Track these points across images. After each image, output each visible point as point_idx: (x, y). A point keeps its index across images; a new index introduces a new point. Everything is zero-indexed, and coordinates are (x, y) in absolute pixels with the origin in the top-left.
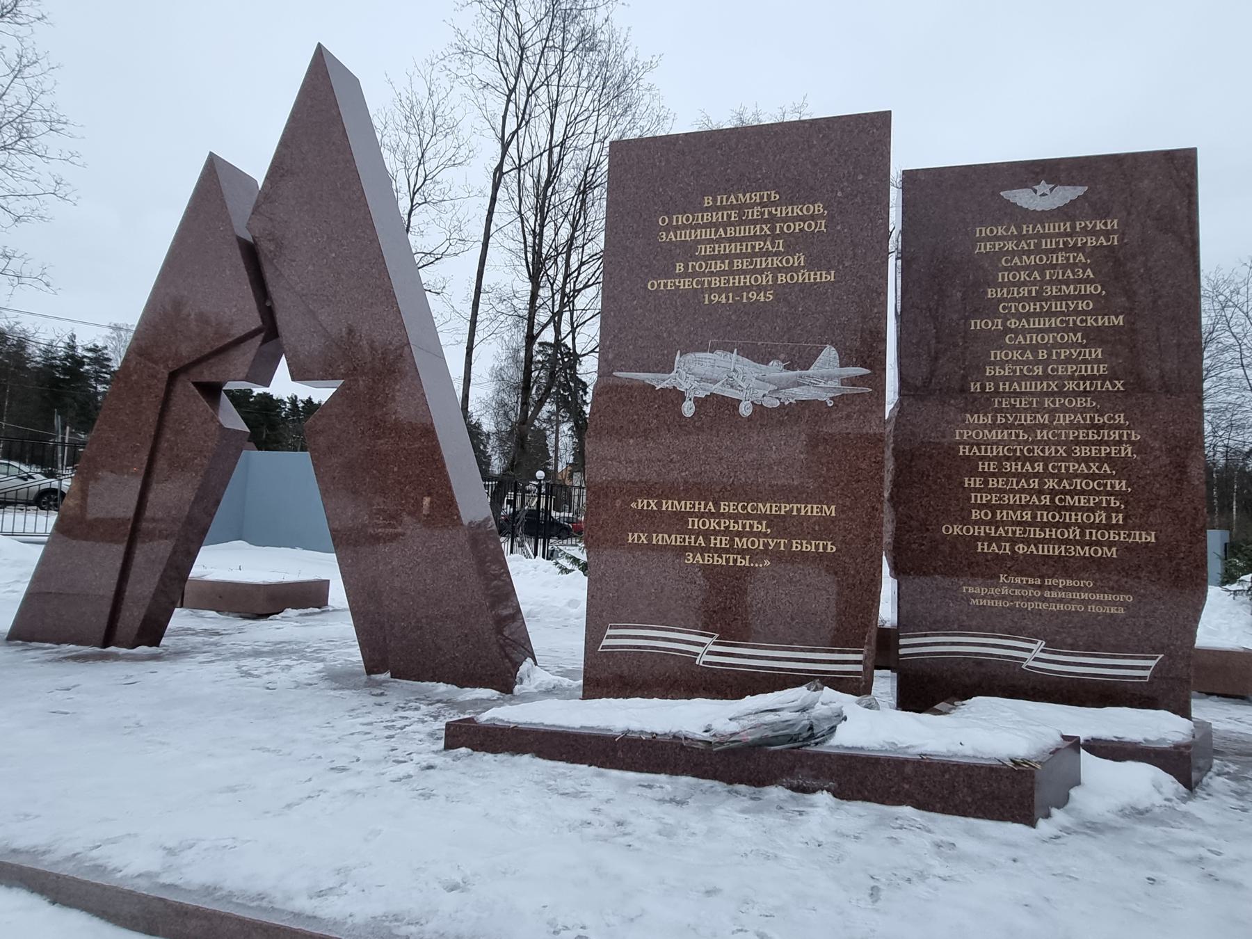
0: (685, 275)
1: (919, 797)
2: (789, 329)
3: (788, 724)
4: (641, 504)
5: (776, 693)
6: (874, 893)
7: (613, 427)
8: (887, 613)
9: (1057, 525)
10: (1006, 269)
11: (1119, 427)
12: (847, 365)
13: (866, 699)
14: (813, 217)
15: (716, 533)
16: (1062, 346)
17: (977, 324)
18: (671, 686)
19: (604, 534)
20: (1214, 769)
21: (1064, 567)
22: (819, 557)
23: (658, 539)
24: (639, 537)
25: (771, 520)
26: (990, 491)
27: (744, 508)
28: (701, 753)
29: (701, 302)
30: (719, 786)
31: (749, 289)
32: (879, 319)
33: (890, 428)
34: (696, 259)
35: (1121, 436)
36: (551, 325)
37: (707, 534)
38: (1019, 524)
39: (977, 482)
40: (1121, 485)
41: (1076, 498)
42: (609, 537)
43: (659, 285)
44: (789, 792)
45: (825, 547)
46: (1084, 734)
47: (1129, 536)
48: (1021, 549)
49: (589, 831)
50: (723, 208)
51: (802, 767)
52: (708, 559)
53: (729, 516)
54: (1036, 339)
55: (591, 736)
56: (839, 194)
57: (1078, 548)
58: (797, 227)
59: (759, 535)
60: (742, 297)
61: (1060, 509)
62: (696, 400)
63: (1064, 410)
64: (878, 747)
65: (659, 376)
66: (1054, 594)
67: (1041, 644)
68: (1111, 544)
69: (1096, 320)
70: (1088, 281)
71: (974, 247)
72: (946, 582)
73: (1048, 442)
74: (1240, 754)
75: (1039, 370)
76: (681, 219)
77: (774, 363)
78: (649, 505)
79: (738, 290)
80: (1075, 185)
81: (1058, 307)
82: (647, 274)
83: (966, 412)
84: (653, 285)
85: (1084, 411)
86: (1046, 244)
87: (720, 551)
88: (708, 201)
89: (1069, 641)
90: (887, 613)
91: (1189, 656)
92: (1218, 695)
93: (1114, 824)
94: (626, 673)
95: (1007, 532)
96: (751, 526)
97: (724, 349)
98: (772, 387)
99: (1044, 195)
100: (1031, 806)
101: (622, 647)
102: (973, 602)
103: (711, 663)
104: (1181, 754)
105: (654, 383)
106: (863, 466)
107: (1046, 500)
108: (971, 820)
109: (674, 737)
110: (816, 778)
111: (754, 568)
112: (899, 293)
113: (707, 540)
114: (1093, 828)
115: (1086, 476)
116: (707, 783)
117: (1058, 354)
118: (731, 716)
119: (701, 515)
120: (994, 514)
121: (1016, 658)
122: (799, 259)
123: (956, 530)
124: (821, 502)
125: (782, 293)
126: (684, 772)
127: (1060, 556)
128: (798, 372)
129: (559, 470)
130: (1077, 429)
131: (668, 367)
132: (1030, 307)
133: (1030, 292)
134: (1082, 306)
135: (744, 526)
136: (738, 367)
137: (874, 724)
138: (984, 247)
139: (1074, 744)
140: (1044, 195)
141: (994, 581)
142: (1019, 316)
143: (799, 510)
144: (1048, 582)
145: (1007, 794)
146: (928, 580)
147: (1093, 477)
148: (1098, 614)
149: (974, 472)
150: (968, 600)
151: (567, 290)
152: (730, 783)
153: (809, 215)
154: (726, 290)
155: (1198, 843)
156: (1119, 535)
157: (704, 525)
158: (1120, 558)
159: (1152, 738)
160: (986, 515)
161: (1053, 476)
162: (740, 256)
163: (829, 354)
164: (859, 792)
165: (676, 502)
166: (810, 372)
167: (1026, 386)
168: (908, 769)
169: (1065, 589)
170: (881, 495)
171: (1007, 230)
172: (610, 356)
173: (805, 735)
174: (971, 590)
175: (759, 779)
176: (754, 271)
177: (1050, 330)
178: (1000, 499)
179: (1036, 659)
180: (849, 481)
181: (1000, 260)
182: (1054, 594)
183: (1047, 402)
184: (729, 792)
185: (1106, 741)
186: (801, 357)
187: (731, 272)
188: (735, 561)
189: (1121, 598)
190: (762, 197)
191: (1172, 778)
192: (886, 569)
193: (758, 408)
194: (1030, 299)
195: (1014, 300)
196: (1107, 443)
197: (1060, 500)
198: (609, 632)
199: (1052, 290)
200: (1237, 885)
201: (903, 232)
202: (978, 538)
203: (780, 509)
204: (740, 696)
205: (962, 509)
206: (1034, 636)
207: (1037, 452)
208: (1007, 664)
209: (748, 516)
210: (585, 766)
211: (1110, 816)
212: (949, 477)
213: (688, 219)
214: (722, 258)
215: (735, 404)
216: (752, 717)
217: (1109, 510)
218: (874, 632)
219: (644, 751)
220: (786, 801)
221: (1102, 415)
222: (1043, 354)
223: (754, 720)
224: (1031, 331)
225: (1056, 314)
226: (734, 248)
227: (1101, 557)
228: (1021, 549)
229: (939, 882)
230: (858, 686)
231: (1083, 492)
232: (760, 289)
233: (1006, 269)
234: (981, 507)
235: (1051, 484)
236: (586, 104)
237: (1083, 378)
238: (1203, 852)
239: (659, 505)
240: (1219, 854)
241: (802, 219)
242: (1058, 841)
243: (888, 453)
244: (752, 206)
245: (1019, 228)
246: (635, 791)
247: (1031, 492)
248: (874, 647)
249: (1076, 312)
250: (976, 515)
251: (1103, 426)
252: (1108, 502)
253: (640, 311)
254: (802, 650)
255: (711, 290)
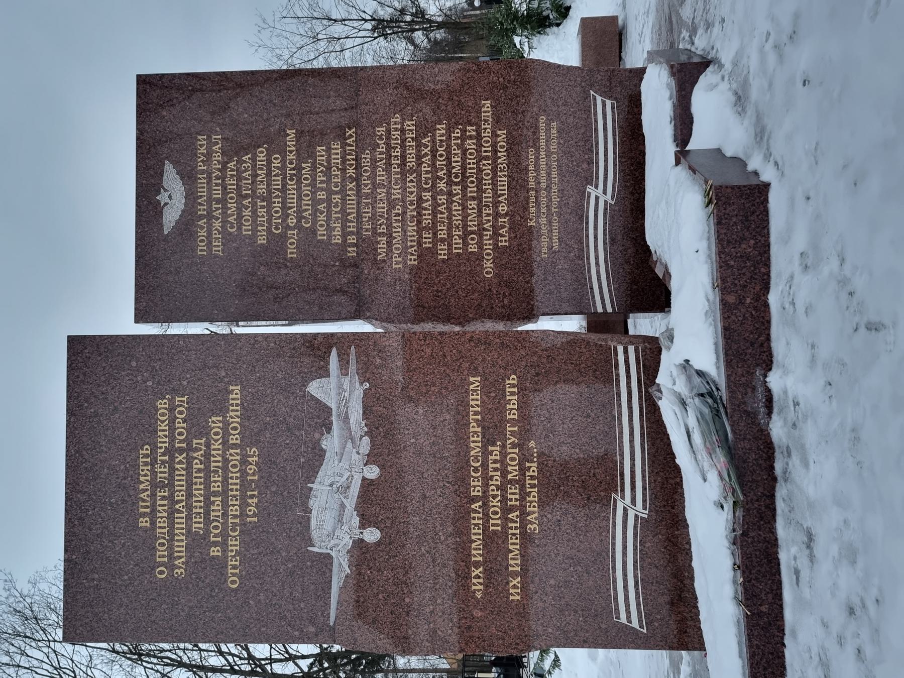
0: (224, 545)
1: (758, 288)
2: (289, 429)
3: (701, 418)
4: (477, 586)
5: (669, 431)
6: (873, 327)
7: (392, 623)
8: (573, 324)
9: (480, 180)
10: (239, 228)
11: (389, 132)
12: (328, 371)
13: (663, 342)
14: (172, 410)
15: (504, 500)
16: (314, 180)
17: (292, 251)
18: (675, 544)
19: (512, 629)
20: (689, 47)
21: (517, 171)
22: (522, 390)
23: (515, 564)
24: (514, 587)
25: (487, 442)
26: (450, 236)
27: (476, 470)
28: (747, 511)
29: (255, 526)
30: (781, 492)
31: (243, 473)
32: (765, 312)
33: (392, 327)
34: (207, 532)
35: (396, 130)
36: (297, 661)
37: (507, 510)
38: (480, 211)
39: (442, 249)
40: (441, 129)
41: (453, 164)
42: (515, 623)
43: (234, 575)
44: (775, 416)
45: (513, 386)
46: (671, 149)
47: (486, 121)
48: (503, 208)
49: (869, 651)
50: (153, 507)
51: (745, 403)
52: (533, 509)
53: (486, 485)
54: (306, 200)
55: (750, 646)
56: (150, 383)
57: (499, 161)
58: (180, 425)
59: (504, 454)
60: (252, 481)
61: (464, 177)
62: (363, 526)
63: (374, 175)
64: (712, 329)
65: (335, 569)
66: (543, 180)
67: (590, 189)
68: (494, 135)
69: (291, 152)
70: (254, 159)
71: (216, 256)
72: (538, 272)
73: (404, 189)
74: (671, 30)
75: (337, 198)
76: (161, 553)
77: (324, 444)
78: (478, 577)
79: (245, 485)
80: (163, 171)
81: (277, 183)
82: (221, 589)
83: (375, 259)
84: (233, 582)
85: (374, 161)
86: (218, 194)
87: (524, 495)
88: (144, 522)
89: (585, 166)
90: (573, 324)
91: (590, 70)
92: (620, 52)
93: (754, 118)
94: (667, 598)
95: (489, 221)
96: (495, 462)
97: (308, 497)
98: (349, 445)
99: (170, 197)
100: (751, 188)
101: (638, 604)
102: (556, 247)
103: (644, 501)
104: (679, 71)
105: (343, 575)
106: (428, 351)
107: (457, 189)
108: (773, 239)
109: (734, 544)
110: (754, 389)
111: (539, 457)
112: (264, 323)
113: (512, 509)
114: (761, 134)
115: (434, 157)
116: (780, 505)
117: (322, 182)
118: (702, 481)
119: (486, 517)
120: (472, 232)
121: (605, 209)
122: (215, 423)
123: (488, 265)
124: (467, 392)
125: (249, 438)
126: (773, 531)
127: (508, 176)
128: (334, 418)
129: (447, 666)
130: (391, 165)
131: (327, 560)
132: (277, 206)
133: (262, 207)
134: (277, 163)
135: (496, 470)
136: (328, 482)
137: (690, 333)
138: (217, 246)
139: (682, 155)
140: (170, 197)
141: (535, 230)
142: (286, 216)
143: (476, 413)
144: (532, 184)
145: (740, 212)
146: (537, 291)
147: (434, 152)
148: (559, 143)
149: (433, 251)
150: (555, 252)
151: (248, 668)
152: (775, 479)
153: (169, 414)
154: (244, 499)
155: (761, 50)
156: (485, 129)
157: (496, 513)
158: (507, 127)
159: (668, 94)
160: (473, 239)
161: (434, 186)
162: (207, 484)
163: (315, 388)
164: (762, 345)
165: (473, 545)
166: (333, 405)
167: (352, 208)
168: (731, 299)
169: (537, 170)
170: (458, 334)
171: (202, 228)
172: (312, 629)
173: (710, 401)
174: (544, 250)
175: (767, 449)
176: (225, 469)
177: (299, 189)
178: (457, 227)
179: (605, 192)
180: (445, 365)
181: (231, 233)
182: (543, 180)
183: (366, 190)
184: (786, 481)
185: (675, 130)
186: (318, 417)
187: (225, 493)
188: (532, 477)
189: (542, 126)
190: (146, 464)
191: (702, 77)
192: (519, 329)
193: (371, 458)
194: (269, 207)
195: (269, 221)
196: (404, 141)
197: (456, 177)
198: (623, 619)
199: (262, 189)
200: (797, 16)
201: (211, 321)
202: (496, 247)
203: (476, 432)
204: (677, 470)
205: (468, 260)
206: (583, 195)
207: (413, 198)
208: (612, 217)
209: (485, 465)
210: (787, 653)
211: (746, 122)
212: (439, 273)
213: (163, 545)
214: (208, 503)
215: (367, 484)
216: (699, 457)
217: (463, 138)
218: (594, 337)
219: (757, 579)
220: (785, 420)
221: (378, 145)
222: (322, 195)
223: (703, 455)
224: (299, 206)
225: (284, 185)
226: (199, 492)
227: (507, 143)
228: (503, 208)
229: (847, 266)
230: (651, 352)
231: (448, 159)
232: (244, 462)
233: (239, 228)
234: (465, 244)
235: (442, 185)
236: (40, 655)
237: (344, 161)
238: (769, 46)
239: (477, 565)
240: (769, 34)
241: (172, 420)
242: (780, 163)
243: (417, 328)
244: (154, 473)
245: (201, 217)
246: (806, 592)
247: (450, 202)
248: (610, 336)
249: (283, 168)
250: (473, 248)
251: (388, 145)
252: (457, 138)
253: (262, 596)
254: (620, 406)
255: (243, 515)
